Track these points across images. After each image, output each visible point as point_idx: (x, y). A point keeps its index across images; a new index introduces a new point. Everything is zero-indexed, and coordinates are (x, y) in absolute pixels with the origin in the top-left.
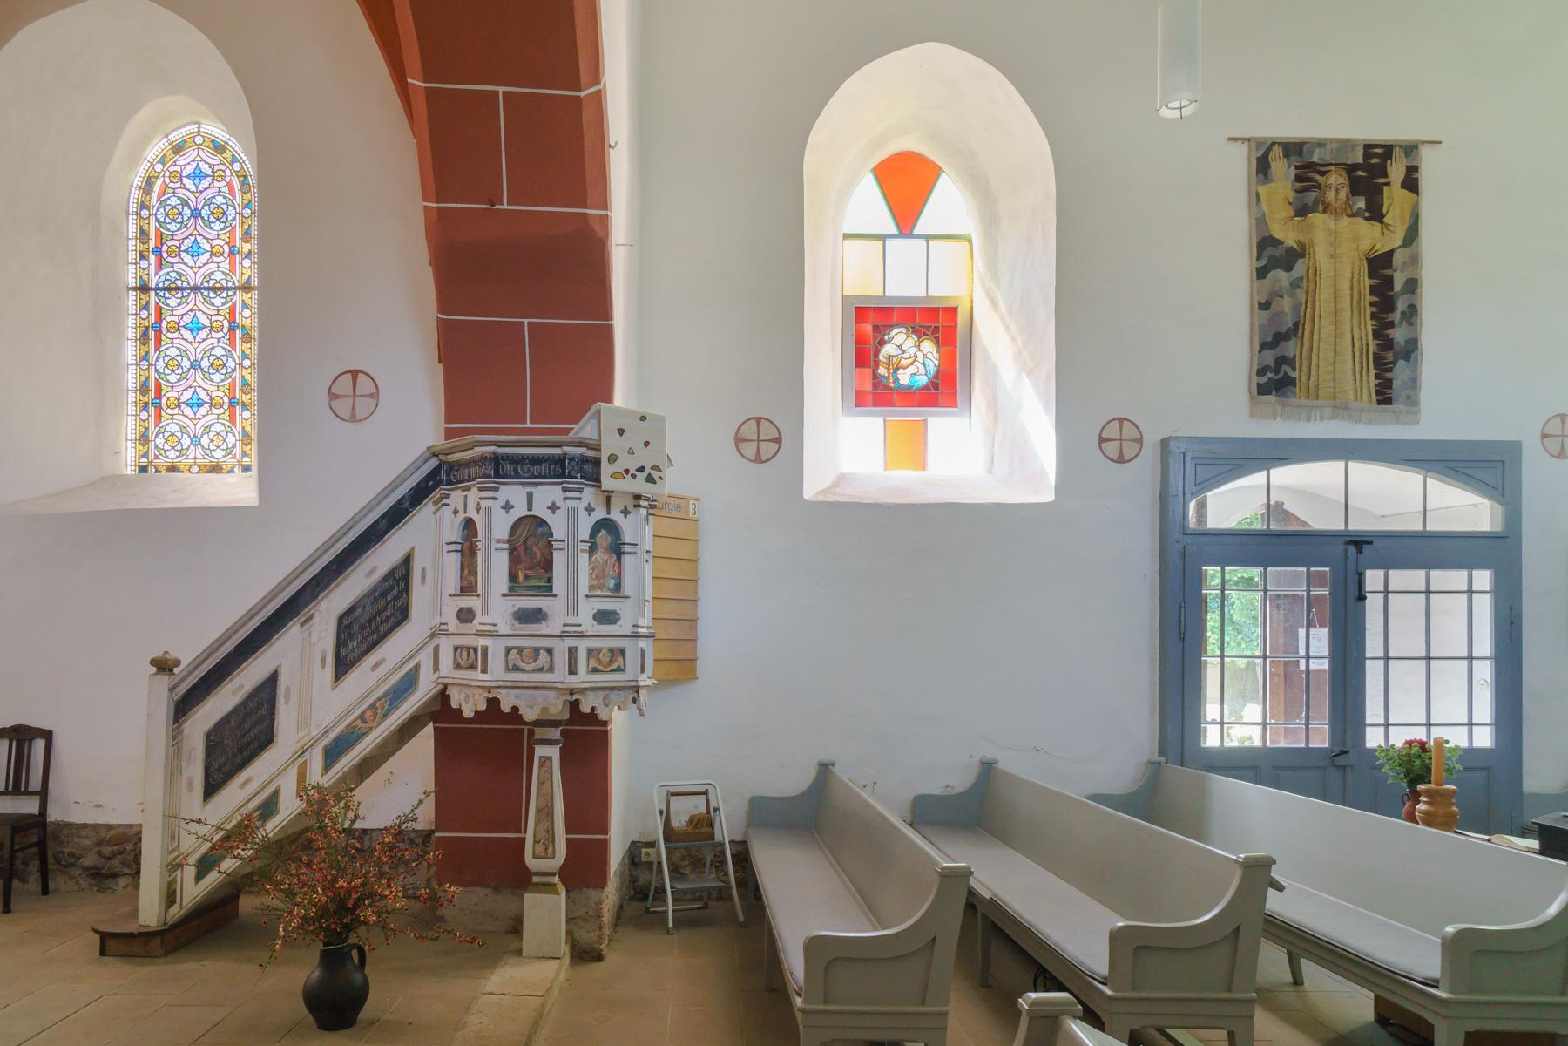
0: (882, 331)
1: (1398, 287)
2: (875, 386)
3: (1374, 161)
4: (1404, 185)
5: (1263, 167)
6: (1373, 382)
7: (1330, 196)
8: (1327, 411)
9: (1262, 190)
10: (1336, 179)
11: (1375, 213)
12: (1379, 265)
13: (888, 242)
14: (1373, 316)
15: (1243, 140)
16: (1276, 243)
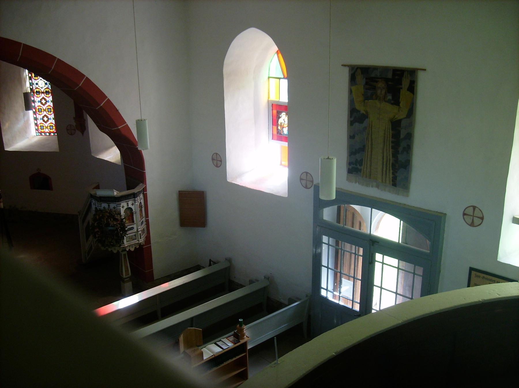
0: (279, 113)
1: (402, 136)
2: (278, 133)
3: (396, 77)
4: (408, 90)
5: (353, 79)
6: (391, 176)
7: (379, 91)
8: (375, 184)
9: (353, 88)
10: (381, 85)
11: (396, 102)
12: (396, 125)
13: (281, 80)
14: (392, 147)
15: (348, 66)
16: (358, 111)
